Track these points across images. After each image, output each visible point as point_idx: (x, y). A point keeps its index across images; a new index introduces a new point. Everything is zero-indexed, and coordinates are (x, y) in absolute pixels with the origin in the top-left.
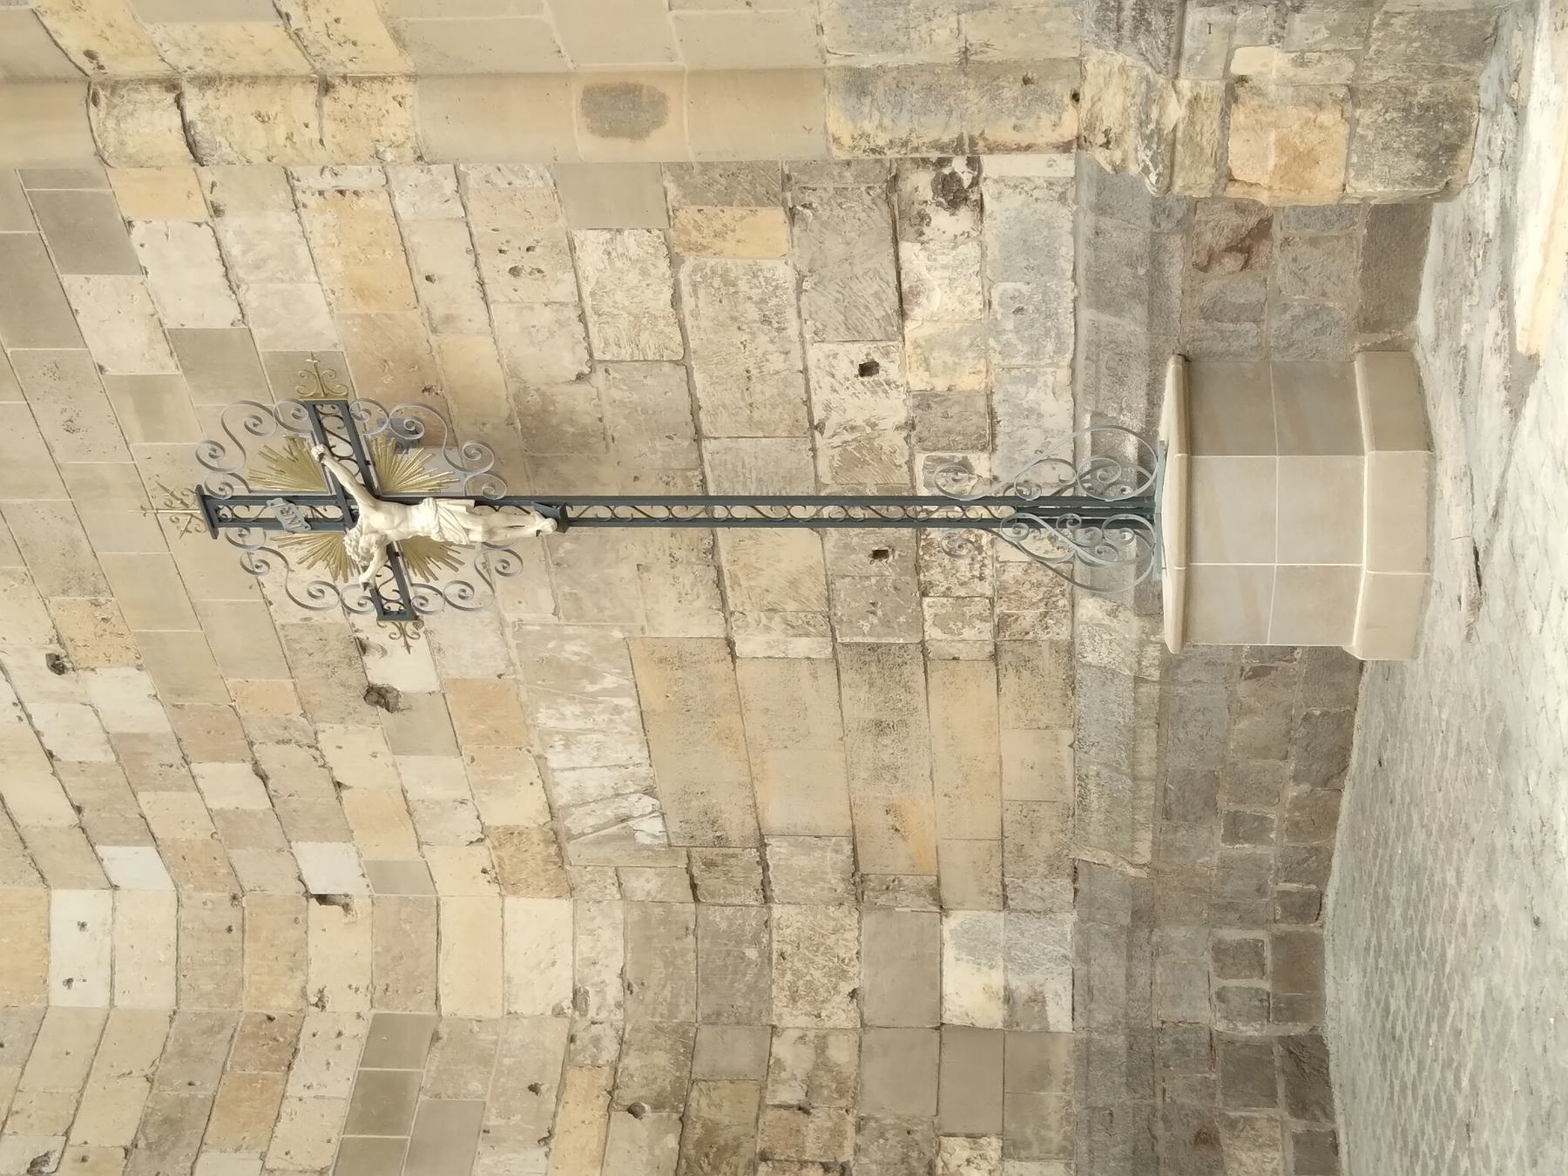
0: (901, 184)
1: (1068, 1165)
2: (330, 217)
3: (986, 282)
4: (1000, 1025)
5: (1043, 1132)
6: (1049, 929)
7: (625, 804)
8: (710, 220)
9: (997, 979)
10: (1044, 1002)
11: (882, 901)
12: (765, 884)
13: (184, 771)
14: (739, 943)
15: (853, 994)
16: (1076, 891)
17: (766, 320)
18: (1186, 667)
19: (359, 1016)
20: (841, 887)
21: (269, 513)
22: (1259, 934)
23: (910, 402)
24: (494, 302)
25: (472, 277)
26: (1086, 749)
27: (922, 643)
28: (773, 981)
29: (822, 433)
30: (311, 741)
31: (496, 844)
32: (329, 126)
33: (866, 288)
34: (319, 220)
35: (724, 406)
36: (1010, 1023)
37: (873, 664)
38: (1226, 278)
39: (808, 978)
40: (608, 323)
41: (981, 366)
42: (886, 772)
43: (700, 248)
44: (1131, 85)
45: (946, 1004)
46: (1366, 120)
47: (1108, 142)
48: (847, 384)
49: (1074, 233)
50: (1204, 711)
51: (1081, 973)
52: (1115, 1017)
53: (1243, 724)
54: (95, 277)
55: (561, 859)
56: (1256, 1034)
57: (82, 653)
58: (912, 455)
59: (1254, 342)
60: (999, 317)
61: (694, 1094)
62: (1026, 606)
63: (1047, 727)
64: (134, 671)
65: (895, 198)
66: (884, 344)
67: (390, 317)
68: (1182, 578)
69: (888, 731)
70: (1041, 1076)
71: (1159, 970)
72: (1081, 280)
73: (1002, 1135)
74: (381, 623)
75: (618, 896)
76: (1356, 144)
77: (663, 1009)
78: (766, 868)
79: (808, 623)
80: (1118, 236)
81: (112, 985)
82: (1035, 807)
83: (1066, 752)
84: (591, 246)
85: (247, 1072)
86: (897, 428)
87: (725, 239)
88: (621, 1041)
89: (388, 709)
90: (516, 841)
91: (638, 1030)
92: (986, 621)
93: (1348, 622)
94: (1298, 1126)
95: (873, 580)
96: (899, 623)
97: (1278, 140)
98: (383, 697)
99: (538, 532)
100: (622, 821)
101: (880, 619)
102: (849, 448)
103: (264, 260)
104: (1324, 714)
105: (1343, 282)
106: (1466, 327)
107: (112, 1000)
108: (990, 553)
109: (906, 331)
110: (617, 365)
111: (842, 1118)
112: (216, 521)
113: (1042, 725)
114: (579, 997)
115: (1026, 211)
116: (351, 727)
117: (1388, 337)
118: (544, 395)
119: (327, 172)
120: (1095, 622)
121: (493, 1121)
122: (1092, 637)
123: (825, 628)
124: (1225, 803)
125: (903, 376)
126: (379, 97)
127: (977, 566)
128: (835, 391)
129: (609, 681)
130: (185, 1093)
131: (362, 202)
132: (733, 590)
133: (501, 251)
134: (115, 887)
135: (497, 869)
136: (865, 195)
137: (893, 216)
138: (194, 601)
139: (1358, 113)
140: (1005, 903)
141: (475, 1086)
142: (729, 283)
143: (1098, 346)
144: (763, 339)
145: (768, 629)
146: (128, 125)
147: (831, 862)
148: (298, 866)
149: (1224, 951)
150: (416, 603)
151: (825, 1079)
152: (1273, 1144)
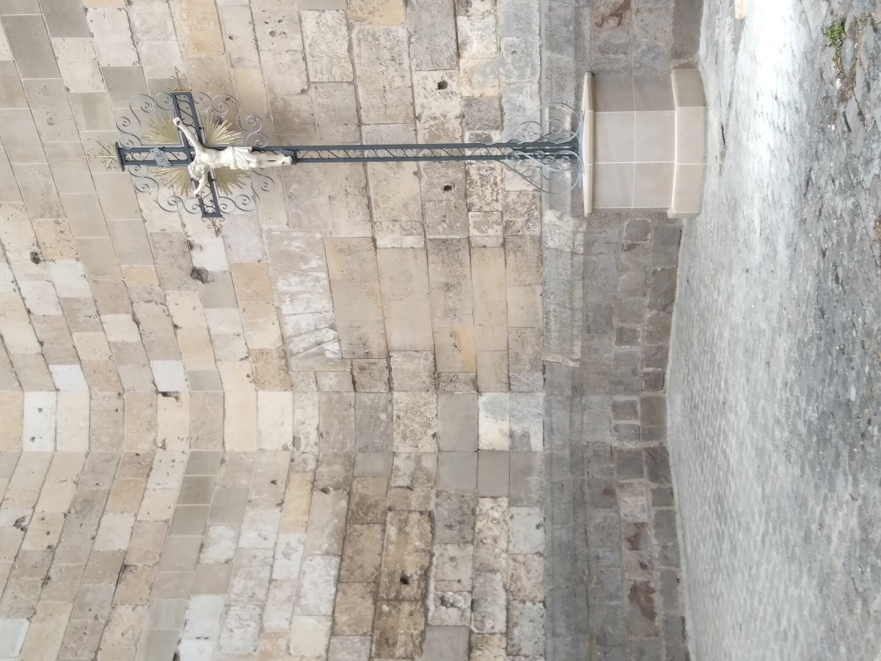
1: (541, 508)
3: (498, 37)
4: (507, 449)
5: (529, 495)
6: (532, 400)
7: (320, 334)
8: (367, 5)
9: (505, 426)
10: (529, 437)
11: (448, 388)
12: (390, 380)
13: (97, 319)
14: (377, 411)
15: (434, 435)
16: (545, 380)
17: (393, 59)
18: (596, 245)
19: (183, 452)
20: (428, 381)
21: (151, 157)
22: (634, 398)
23: (462, 103)
24: (262, 50)
26: (548, 296)
27: (468, 238)
28: (394, 430)
29: (420, 121)
30: (163, 301)
31: (255, 359)
33: (442, 41)
35: (373, 107)
36: (512, 447)
38: (610, 33)
39: (412, 428)
40: (317, 61)
42: (450, 313)
43: (361, 20)
45: (481, 439)
48: (432, 93)
49: (540, 10)
50: (604, 269)
51: (548, 420)
52: (564, 442)
53: (624, 277)
54: (67, 39)
55: (287, 368)
56: (633, 447)
57: (49, 251)
58: (463, 133)
59: (624, 65)
60: (504, 56)
61: (355, 483)
62: (519, 216)
64: (74, 262)
66: (449, 71)
67: (211, 59)
68: (592, 170)
69: (451, 289)
70: (528, 470)
71: (586, 417)
72: (543, 36)
73: (508, 496)
74: (204, 219)
75: (315, 389)
77: (339, 445)
78: (390, 370)
79: (412, 228)
80: (560, 11)
81: (56, 440)
82: (524, 331)
83: (539, 299)
84: (310, 18)
85: (127, 478)
86: (457, 117)
87: (374, 15)
88: (318, 461)
90: (264, 357)
91: (326, 456)
93: (668, 193)
94: (654, 486)
95: (444, 203)
96: (457, 227)
98: (200, 275)
99: (283, 163)
100: (319, 344)
102: (433, 129)
103: (151, 29)
104: (663, 270)
105: (665, 32)
106: (717, 31)
107: (55, 448)
109: (460, 64)
111: (429, 491)
112: (124, 162)
113: (527, 283)
114: (296, 440)
116: (183, 292)
117: (686, 61)
118: (284, 101)
120: (552, 223)
121: (253, 497)
122: (551, 232)
123: (421, 230)
124: (616, 323)
125: (459, 89)
127: (495, 194)
129: (314, 263)
130: (95, 488)
134: (58, 390)
135: (255, 375)
138: (107, 220)
140: (509, 387)
141: (244, 482)
143: (552, 71)
144: (392, 69)
145: (393, 231)
147: (423, 365)
149: (618, 407)
150: (221, 207)
151: (420, 474)
152: (642, 494)
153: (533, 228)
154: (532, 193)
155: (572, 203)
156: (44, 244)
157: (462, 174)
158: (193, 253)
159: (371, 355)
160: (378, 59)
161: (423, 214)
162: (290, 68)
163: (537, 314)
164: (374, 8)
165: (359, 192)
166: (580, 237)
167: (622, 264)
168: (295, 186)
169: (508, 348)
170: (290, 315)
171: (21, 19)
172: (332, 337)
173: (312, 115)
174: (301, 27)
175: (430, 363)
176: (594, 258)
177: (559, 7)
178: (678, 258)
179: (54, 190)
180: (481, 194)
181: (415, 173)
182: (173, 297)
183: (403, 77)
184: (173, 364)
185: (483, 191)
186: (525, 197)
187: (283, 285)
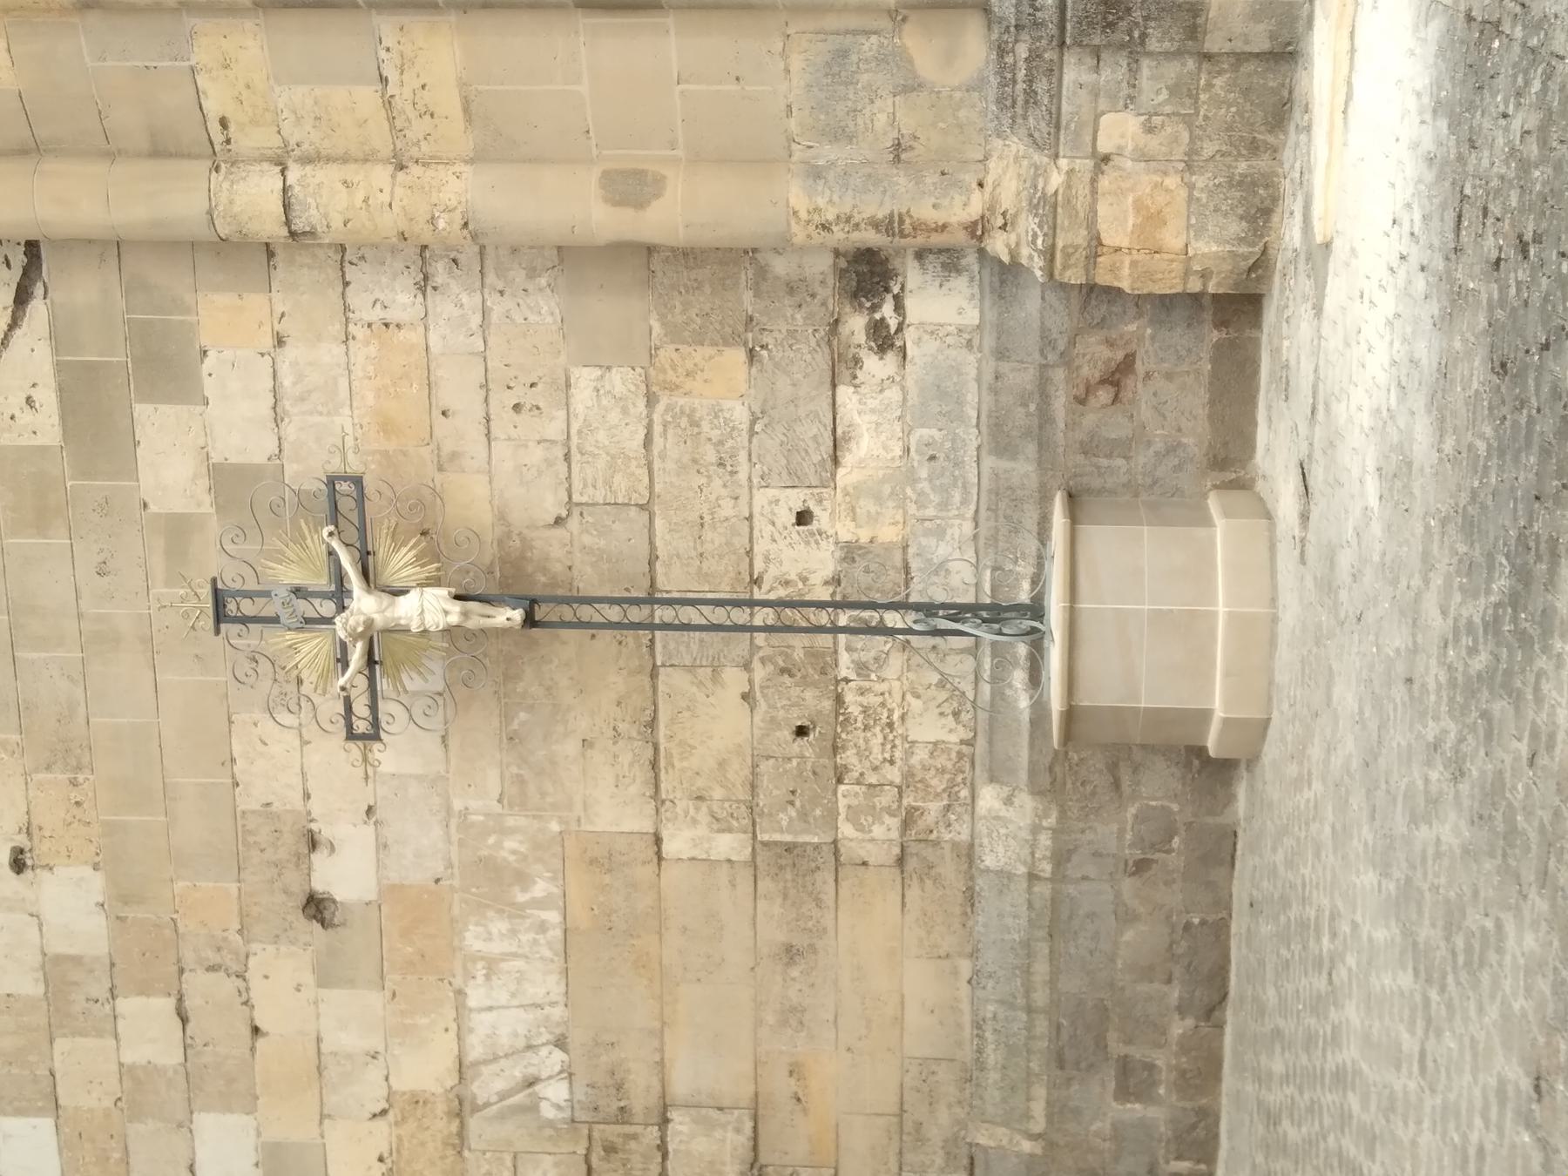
0: (840, 329)
2: (372, 350)
8: (684, 359)
13: (108, 1007)
17: (721, 464)
18: (1075, 859)
23: (838, 554)
25: (481, 414)
26: (983, 981)
27: (835, 842)
32: (399, 191)
34: (363, 352)
35: (678, 556)
37: (788, 869)
41: (899, 518)
42: (793, 1016)
43: (672, 388)
44: (1023, 171)
46: (1200, 184)
47: (1006, 224)
48: (785, 533)
49: (978, 380)
50: (1091, 916)
53: (1129, 935)
54: (163, 408)
55: (460, 1142)
59: (1124, 479)
60: (916, 464)
63: (948, 956)
64: (88, 871)
65: (835, 343)
66: (816, 491)
67: (405, 454)
68: (1067, 616)
69: (797, 958)
72: (984, 429)
76: (1194, 207)
78: (665, 1156)
82: (934, 1068)
83: (965, 990)
84: (584, 378)
86: (826, 583)
89: (323, 925)
92: (894, 816)
95: (795, 762)
96: (815, 818)
97: (1135, 202)
98: (321, 913)
101: (797, 811)
103: (309, 392)
104: (1203, 923)
105: (1195, 418)
108: (900, 732)
110: (591, 508)
113: (942, 953)
115: (940, 357)
116: (283, 949)
117: (1234, 476)
118: (523, 539)
119: (378, 305)
120: (993, 814)
122: (990, 835)
123: (746, 822)
124: (1116, 1047)
126: (444, 173)
128: (775, 541)
129: (540, 888)
131: (402, 334)
132: (667, 772)
133: (509, 388)
136: (811, 337)
137: (833, 359)
138: (167, 780)
139: (1194, 178)
142: (695, 423)
143: (997, 494)
144: (717, 482)
146: (240, 187)
148: (193, 1148)
153: (956, 826)
154: (957, 748)
155: (1031, 762)
156: (41, 829)
157: (830, 702)
158: (316, 858)
159: (631, 1115)
160: (695, 461)
161: (753, 787)
162: (540, 473)
163: (959, 1026)
164: (695, 365)
165: (639, 733)
166: (1045, 840)
167: (1126, 905)
168: (523, 716)
169: (902, 1110)
170: (481, 1010)
171: (90, 367)
172: (557, 1068)
173: (570, 568)
174: (567, 398)
175: (743, 1140)
176: (1071, 889)
177: (1013, 370)
178: (1231, 896)
179: (82, 710)
180: (863, 747)
181: (745, 697)
182: (263, 957)
183: (736, 498)
184: (238, 1122)
185: (867, 741)
186: (945, 756)
187: (477, 937)
